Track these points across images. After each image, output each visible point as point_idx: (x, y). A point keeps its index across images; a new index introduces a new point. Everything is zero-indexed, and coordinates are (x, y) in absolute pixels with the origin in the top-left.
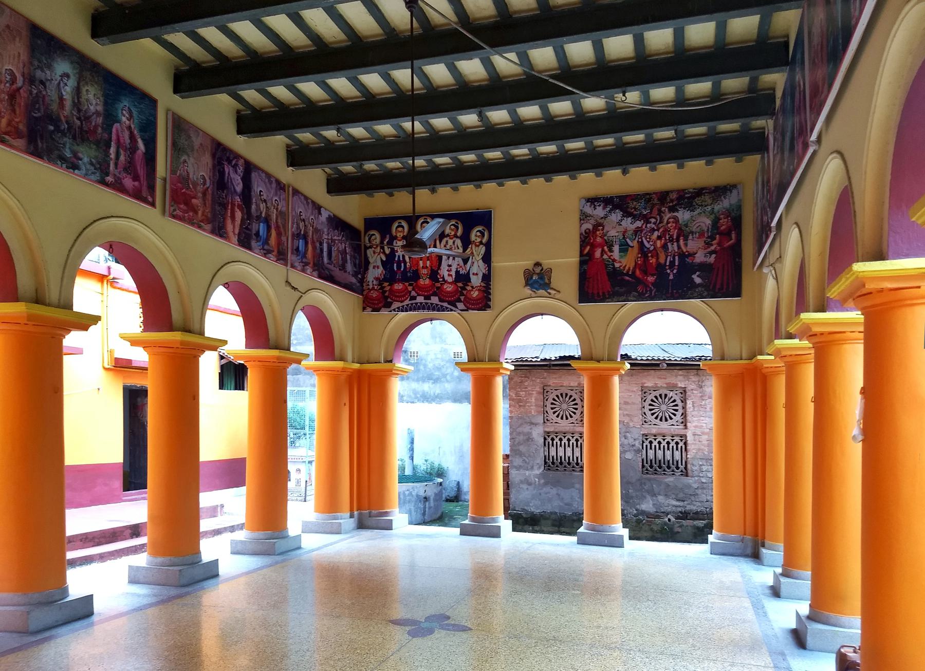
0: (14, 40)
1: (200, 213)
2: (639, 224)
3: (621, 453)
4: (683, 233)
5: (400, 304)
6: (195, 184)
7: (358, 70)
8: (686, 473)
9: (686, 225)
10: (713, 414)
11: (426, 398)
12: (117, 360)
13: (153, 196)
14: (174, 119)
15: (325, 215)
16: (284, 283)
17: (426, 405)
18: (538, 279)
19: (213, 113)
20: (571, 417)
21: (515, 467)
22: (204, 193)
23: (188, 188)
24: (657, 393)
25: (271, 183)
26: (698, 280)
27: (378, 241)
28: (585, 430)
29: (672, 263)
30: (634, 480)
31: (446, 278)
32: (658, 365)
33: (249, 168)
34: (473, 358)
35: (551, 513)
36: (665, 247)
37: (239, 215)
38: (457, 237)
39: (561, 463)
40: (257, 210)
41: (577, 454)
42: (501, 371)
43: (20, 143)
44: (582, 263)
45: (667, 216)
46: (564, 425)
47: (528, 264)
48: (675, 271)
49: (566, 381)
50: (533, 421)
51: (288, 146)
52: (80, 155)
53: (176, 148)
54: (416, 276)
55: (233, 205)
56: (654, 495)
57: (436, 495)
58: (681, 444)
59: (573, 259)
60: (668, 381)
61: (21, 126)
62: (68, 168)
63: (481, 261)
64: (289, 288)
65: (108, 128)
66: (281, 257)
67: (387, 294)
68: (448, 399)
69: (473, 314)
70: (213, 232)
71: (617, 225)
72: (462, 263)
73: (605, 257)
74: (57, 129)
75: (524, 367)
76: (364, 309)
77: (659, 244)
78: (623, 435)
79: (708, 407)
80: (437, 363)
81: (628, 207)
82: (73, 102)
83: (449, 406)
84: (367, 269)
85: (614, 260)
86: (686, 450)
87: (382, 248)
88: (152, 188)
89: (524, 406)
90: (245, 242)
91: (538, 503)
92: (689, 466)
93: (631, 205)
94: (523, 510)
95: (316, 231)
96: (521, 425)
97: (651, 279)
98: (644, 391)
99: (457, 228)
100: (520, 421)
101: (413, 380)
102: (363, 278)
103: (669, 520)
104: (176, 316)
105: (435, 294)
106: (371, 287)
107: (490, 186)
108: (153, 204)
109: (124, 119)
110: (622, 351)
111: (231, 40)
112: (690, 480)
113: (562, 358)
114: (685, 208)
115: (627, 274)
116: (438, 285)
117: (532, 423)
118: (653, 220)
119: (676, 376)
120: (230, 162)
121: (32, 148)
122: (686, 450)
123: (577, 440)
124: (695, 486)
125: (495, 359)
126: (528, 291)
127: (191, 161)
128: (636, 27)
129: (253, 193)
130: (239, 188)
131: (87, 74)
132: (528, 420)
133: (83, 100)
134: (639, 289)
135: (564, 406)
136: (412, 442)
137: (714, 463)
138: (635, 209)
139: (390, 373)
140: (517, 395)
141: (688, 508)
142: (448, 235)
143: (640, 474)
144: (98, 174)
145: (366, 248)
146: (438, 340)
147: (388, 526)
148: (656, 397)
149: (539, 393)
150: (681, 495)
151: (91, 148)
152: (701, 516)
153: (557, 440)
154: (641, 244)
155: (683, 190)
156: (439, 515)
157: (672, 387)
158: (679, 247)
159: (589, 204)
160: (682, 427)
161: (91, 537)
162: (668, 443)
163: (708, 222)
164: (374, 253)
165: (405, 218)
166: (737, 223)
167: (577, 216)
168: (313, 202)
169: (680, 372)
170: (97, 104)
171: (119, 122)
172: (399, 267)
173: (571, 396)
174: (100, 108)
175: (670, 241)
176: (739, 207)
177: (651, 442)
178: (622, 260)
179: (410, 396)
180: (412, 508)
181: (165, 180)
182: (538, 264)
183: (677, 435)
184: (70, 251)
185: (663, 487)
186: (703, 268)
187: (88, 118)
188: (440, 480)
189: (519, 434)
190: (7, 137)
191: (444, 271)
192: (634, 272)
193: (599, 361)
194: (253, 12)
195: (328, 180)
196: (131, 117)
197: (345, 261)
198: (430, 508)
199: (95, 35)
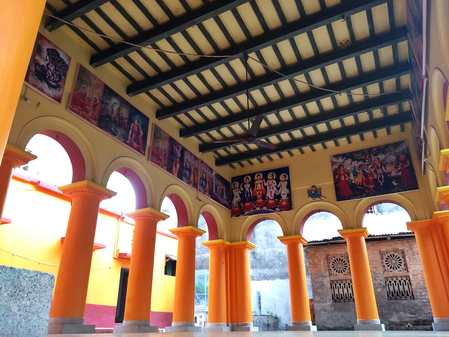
1: (163, 162)
2: (361, 163)
3: (375, 289)
4: (383, 164)
5: (248, 212)
6: (162, 151)
8: (413, 298)
9: (384, 161)
10: (421, 263)
11: (266, 277)
12: (120, 254)
13: (145, 151)
16: (195, 198)
17: (266, 281)
18: (315, 193)
21: (317, 302)
22: (165, 155)
23: (159, 151)
24: (389, 254)
25: (192, 156)
26: (395, 184)
27: (238, 186)
28: (352, 277)
29: (381, 178)
31: (270, 197)
33: (184, 150)
36: (375, 171)
37: (178, 166)
41: (350, 291)
43: (95, 122)
44: (335, 183)
46: (341, 276)
47: (309, 187)
48: (383, 181)
49: (338, 252)
50: (324, 275)
52: (118, 131)
54: (256, 198)
55: (176, 161)
56: (397, 312)
57: (274, 323)
58: (407, 281)
59: (331, 182)
60: (393, 247)
61: (96, 117)
64: (197, 200)
65: (129, 124)
66: (195, 185)
68: (278, 277)
70: (167, 170)
71: (349, 165)
72: (276, 190)
73: (347, 179)
74: (110, 120)
75: (314, 246)
76: (232, 216)
77: (372, 170)
78: (374, 279)
79: (418, 259)
80: (270, 258)
81: (354, 157)
83: (278, 282)
84: (233, 198)
85: (351, 180)
86: (410, 284)
87: (240, 188)
88: (144, 149)
89: (318, 267)
90: (180, 176)
91: (331, 322)
92: (414, 293)
93: (355, 156)
95: (210, 178)
96: (317, 278)
97: (372, 186)
98: (382, 254)
99: (273, 175)
101: (259, 268)
102: (231, 202)
103: (409, 326)
105: (265, 206)
106: (235, 206)
108: (144, 155)
109: (136, 122)
112: (416, 302)
115: (359, 185)
116: (266, 201)
118: (367, 161)
119: (397, 244)
120: (176, 146)
122: (410, 284)
123: (349, 284)
124: (420, 304)
126: (310, 199)
127: (161, 142)
130: (179, 155)
133: (121, 112)
134: (367, 191)
135: (340, 266)
136: (260, 299)
137: (428, 290)
138: (358, 157)
140: (313, 261)
141: (419, 318)
142: (269, 179)
143: (387, 300)
145: (232, 189)
146: (270, 246)
147: (248, 329)
149: (324, 259)
150: (413, 311)
152: (427, 323)
153: (338, 285)
154: (364, 172)
157: (396, 250)
158: (382, 170)
160: (405, 271)
162: (400, 281)
163: (394, 158)
164: (236, 191)
165: (249, 175)
166: (408, 156)
169: (399, 242)
171: (134, 123)
172: (247, 196)
173: (342, 260)
174: (127, 117)
175: (377, 168)
176: (408, 150)
179: (257, 277)
181: (150, 148)
182: (314, 186)
183: (404, 276)
185: (401, 307)
186: (396, 178)
187: (122, 119)
191: (268, 195)
192: (362, 184)
196: (139, 122)
197: (223, 194)
199: (127, 93)
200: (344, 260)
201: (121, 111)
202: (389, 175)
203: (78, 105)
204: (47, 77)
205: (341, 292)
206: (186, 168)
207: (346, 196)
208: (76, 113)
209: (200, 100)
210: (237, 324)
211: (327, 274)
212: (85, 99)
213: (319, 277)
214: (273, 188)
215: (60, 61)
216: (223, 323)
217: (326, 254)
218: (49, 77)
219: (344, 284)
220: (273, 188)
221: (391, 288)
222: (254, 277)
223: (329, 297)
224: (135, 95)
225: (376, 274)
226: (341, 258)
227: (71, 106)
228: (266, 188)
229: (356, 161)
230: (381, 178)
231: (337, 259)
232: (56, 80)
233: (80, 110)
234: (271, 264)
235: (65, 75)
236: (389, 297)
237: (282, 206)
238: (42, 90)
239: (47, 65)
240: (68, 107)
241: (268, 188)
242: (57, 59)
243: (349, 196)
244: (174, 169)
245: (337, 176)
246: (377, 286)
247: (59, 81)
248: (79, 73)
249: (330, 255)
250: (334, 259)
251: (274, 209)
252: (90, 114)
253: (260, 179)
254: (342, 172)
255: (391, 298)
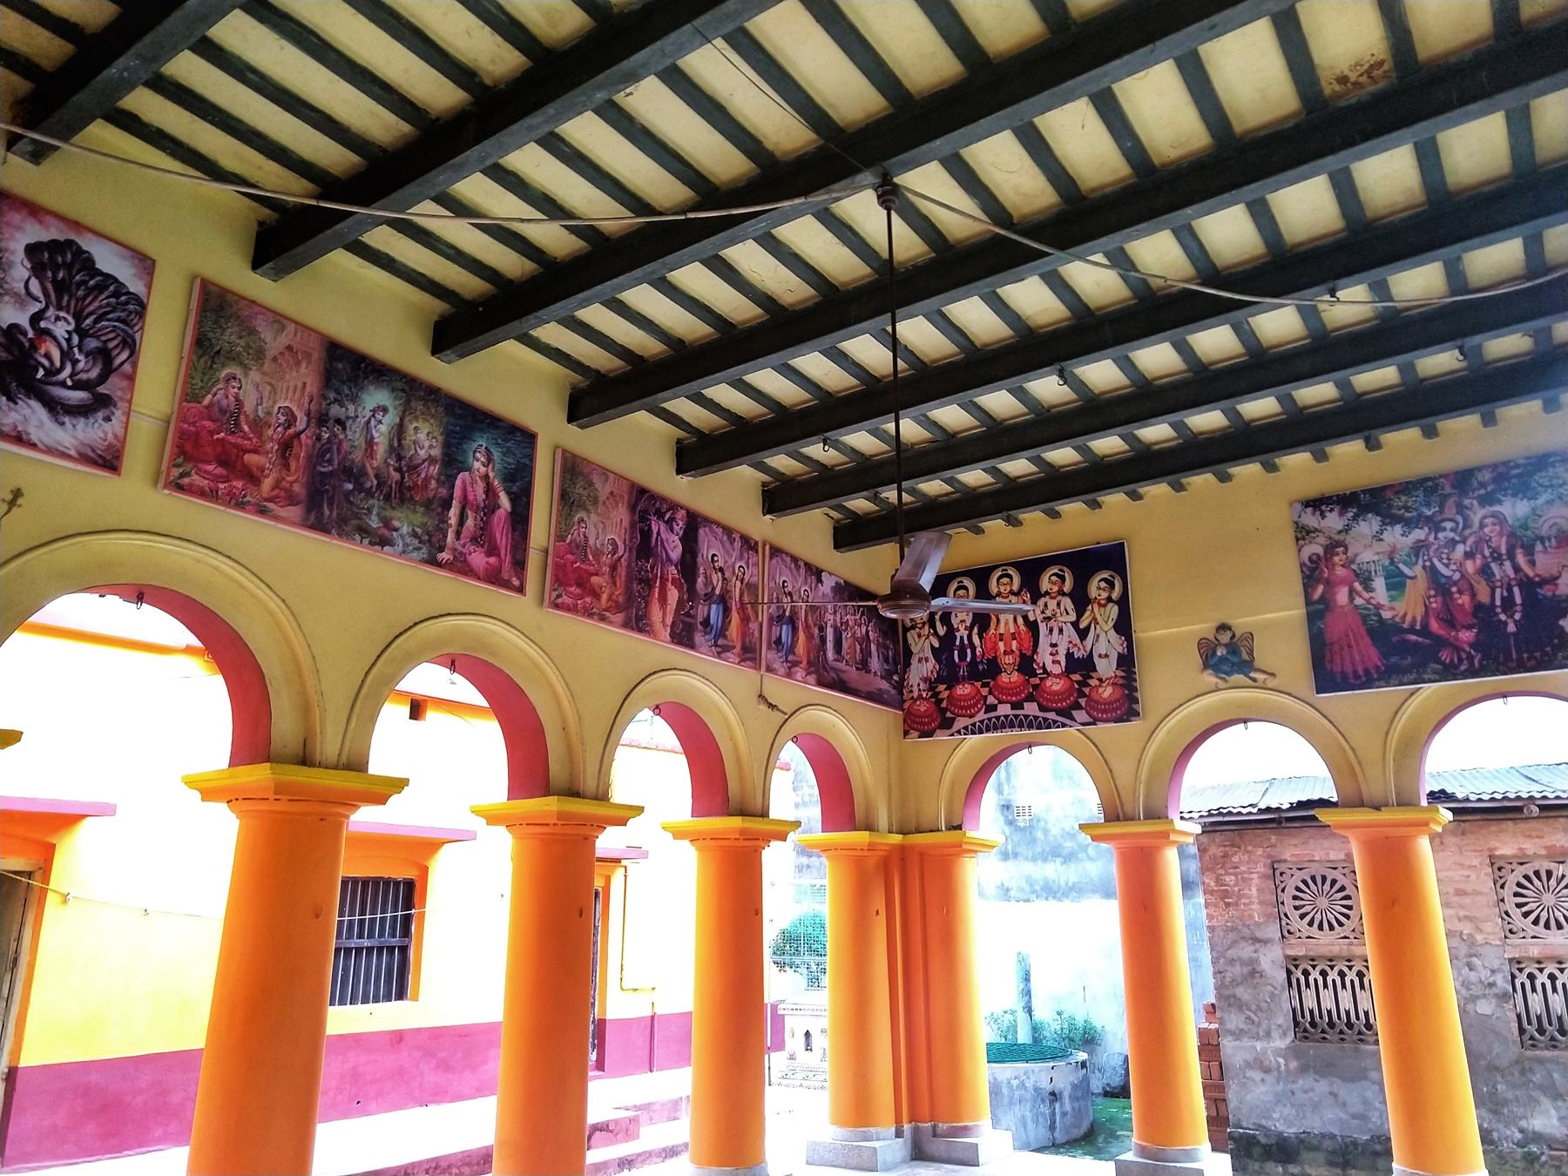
0: (298, 363)
1: (604, 597)
2: (1419, 534)
5: (968, 721)
6: (598, 554)
7: (835, 335)
9: (1525, 527)
11: (1051, 891)
14: (564, 459)
15: (828, 583)
18: (1227, 655)
19: (635, 444)
20: (1341, 924)
21: (1232, 1033)
22: (613, 568)
23: (585, 560)
28: (1369, 949)
29: (1508, 604)
30: (1504, 1063)
32: (1519, 809)
33: (695, 522)
34: (1115, 812)
35: (1323, 1136)
36: (1485, 571)
37: (673, 595)
38: (1064, 594)
39: (1331, 1024)
40: (706, 585)
42: (1172, 837)
43: (295, 512)
45: (1478, 514)
47: (1205, 628)
48: (1517, 616)
50: (1259, 935)
51: (764, 484)
52: (396, 523)
53: (567, 501)
54: (994, 668)
57: (1075, 1087)
60: (1547, 841)
61: (297, 488)
62: (371, 543)
63: (1112, 634)
64: (763, 707)
65: (449, 481)
66: (749, 654)
67: (944, 705)
68: (1094, 891)
69: (1106, 732)
70: (626, 625)
71: (1370, 542)
72: (1076, 639)
73: (1358, 601)
74: (359, 487)
75: (1227, 829)
76: (906, 733)
77: (1470, 566)
78: (1465, 956)
82: (391, 446)
84: (908, 664)
85: (1378, 607)
88: (520, 565)
89: (1237, 904)
90: (683, 636)
93: (1397, 503)
94: (1260, 1127)
96: (1234, 943)
97: (1466, 636)
98: (1497, 866)
99: (1063, 579)
100: (1231, 936)
101: (1026, 859)
102: (903, 679)
104: (556, 769)
105: (1030, 698)
106: (916, 695)
107: (1114, 499)
108: (521, 590)
109: (477, 465)
110: (1430, 785)
111: (640, 327)
113: (1301, 805)
114: (1514, 495)
115: (1412, 630)
117: (1256, 940)
118: (1449, 525)
120: (660, 515)
121: (312, 518)
125: (1156, 814)
126: (1210, 679)
128: (1330, 159)
129: (699, 559)
130: (676, 552)
131: (419, 406)
132: (1246, 932)
133: (407, 442)
134: (1445, 655)
135: (1323, 902)
136: (1027, 978)
138: (1407, 509)
139: (960, 850)
140: (1218, 881)
142: (1047, 593)
143: (1515, 1049)
144: (424, 550)
148: (1526, 877)
149: (1264, 877)
151: (415, 512)
154: (1432, 572)
155: (1505, 464)
156: (1085, 1126)
158: (1517, 569)
159: (1309, 510)
161: (443, 1164)
164: (919, 636)
165: (969, 573)
167: (1290, 534)
168: (806, 564)
170: (431, 447)
171: (469, 469)
172: (963, 656)
173: (1334, 882)
174: (436, 452)
175: (1495, 559)
177: (1531, 977)
178: (1396, 604)
180: (1028, 1115)
182: (1223, 627)
184: (367, 673)
187: (414, 468)
188: (1082, 1056)
189: (1232, 961)
190: (271, 505)
191: (1044, 656)
192: (1425, 625)
193: (1377, 808)
194: (647, 268)
195: (835, 528)
196: (489, 460)
197: (866, 654)
198: (1064, 1114)
200: (1342, 880)
201: (410, 435)
202: (1546, 591)
203: (209, 457)
204: (41, 373)
205: (1328, 1002)
206: (708, 597)
207: (1355, 672)
208: (202, 494)
209: (730, 347)
210: (934, 1127)
211: (1273, 931)
212: (237, 425)
213: (1243, 944)
214: (1061, 631)
215: (101, 288)
216: (879, 1129)
217: (1269, 856)
218: (52, 372)
219: (1342, 974)
220: (1061, 631)
221: (1536, 1002)
222: (1008, 890)
223: (1280, 1021)
224: (462, 356)
225: (1472, 943)
226: (1331, 875)
227: (176, 472)
228: (1033, 627)
229: (1398, 528)
230: (1508, 604)
231: (1313, 878)
232: (84, 376)
233: (217, 479)
234: (1068, 844)
235: (130, 344)
236: (1526, 1037)
237: (1097, 702)
238: (19, 439)
239: (35, 319)
240: (163, 476)
241: (1043, 628)
242: (84, 283)
243: (1367, 672)
244: (656, 613)
245: (1320, 589)
246: (1476, 991)
247: (103, 378)
248: (200, 323)
249: (1285, 861)
250: (1299, 875)
251: (1066, 713)
252: (267, 484)
253: (1012, 593)
254: (1340, 571)
255: (1532, 1038)
